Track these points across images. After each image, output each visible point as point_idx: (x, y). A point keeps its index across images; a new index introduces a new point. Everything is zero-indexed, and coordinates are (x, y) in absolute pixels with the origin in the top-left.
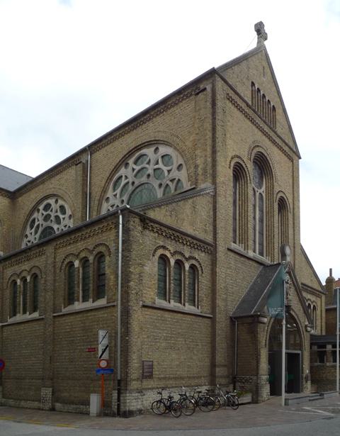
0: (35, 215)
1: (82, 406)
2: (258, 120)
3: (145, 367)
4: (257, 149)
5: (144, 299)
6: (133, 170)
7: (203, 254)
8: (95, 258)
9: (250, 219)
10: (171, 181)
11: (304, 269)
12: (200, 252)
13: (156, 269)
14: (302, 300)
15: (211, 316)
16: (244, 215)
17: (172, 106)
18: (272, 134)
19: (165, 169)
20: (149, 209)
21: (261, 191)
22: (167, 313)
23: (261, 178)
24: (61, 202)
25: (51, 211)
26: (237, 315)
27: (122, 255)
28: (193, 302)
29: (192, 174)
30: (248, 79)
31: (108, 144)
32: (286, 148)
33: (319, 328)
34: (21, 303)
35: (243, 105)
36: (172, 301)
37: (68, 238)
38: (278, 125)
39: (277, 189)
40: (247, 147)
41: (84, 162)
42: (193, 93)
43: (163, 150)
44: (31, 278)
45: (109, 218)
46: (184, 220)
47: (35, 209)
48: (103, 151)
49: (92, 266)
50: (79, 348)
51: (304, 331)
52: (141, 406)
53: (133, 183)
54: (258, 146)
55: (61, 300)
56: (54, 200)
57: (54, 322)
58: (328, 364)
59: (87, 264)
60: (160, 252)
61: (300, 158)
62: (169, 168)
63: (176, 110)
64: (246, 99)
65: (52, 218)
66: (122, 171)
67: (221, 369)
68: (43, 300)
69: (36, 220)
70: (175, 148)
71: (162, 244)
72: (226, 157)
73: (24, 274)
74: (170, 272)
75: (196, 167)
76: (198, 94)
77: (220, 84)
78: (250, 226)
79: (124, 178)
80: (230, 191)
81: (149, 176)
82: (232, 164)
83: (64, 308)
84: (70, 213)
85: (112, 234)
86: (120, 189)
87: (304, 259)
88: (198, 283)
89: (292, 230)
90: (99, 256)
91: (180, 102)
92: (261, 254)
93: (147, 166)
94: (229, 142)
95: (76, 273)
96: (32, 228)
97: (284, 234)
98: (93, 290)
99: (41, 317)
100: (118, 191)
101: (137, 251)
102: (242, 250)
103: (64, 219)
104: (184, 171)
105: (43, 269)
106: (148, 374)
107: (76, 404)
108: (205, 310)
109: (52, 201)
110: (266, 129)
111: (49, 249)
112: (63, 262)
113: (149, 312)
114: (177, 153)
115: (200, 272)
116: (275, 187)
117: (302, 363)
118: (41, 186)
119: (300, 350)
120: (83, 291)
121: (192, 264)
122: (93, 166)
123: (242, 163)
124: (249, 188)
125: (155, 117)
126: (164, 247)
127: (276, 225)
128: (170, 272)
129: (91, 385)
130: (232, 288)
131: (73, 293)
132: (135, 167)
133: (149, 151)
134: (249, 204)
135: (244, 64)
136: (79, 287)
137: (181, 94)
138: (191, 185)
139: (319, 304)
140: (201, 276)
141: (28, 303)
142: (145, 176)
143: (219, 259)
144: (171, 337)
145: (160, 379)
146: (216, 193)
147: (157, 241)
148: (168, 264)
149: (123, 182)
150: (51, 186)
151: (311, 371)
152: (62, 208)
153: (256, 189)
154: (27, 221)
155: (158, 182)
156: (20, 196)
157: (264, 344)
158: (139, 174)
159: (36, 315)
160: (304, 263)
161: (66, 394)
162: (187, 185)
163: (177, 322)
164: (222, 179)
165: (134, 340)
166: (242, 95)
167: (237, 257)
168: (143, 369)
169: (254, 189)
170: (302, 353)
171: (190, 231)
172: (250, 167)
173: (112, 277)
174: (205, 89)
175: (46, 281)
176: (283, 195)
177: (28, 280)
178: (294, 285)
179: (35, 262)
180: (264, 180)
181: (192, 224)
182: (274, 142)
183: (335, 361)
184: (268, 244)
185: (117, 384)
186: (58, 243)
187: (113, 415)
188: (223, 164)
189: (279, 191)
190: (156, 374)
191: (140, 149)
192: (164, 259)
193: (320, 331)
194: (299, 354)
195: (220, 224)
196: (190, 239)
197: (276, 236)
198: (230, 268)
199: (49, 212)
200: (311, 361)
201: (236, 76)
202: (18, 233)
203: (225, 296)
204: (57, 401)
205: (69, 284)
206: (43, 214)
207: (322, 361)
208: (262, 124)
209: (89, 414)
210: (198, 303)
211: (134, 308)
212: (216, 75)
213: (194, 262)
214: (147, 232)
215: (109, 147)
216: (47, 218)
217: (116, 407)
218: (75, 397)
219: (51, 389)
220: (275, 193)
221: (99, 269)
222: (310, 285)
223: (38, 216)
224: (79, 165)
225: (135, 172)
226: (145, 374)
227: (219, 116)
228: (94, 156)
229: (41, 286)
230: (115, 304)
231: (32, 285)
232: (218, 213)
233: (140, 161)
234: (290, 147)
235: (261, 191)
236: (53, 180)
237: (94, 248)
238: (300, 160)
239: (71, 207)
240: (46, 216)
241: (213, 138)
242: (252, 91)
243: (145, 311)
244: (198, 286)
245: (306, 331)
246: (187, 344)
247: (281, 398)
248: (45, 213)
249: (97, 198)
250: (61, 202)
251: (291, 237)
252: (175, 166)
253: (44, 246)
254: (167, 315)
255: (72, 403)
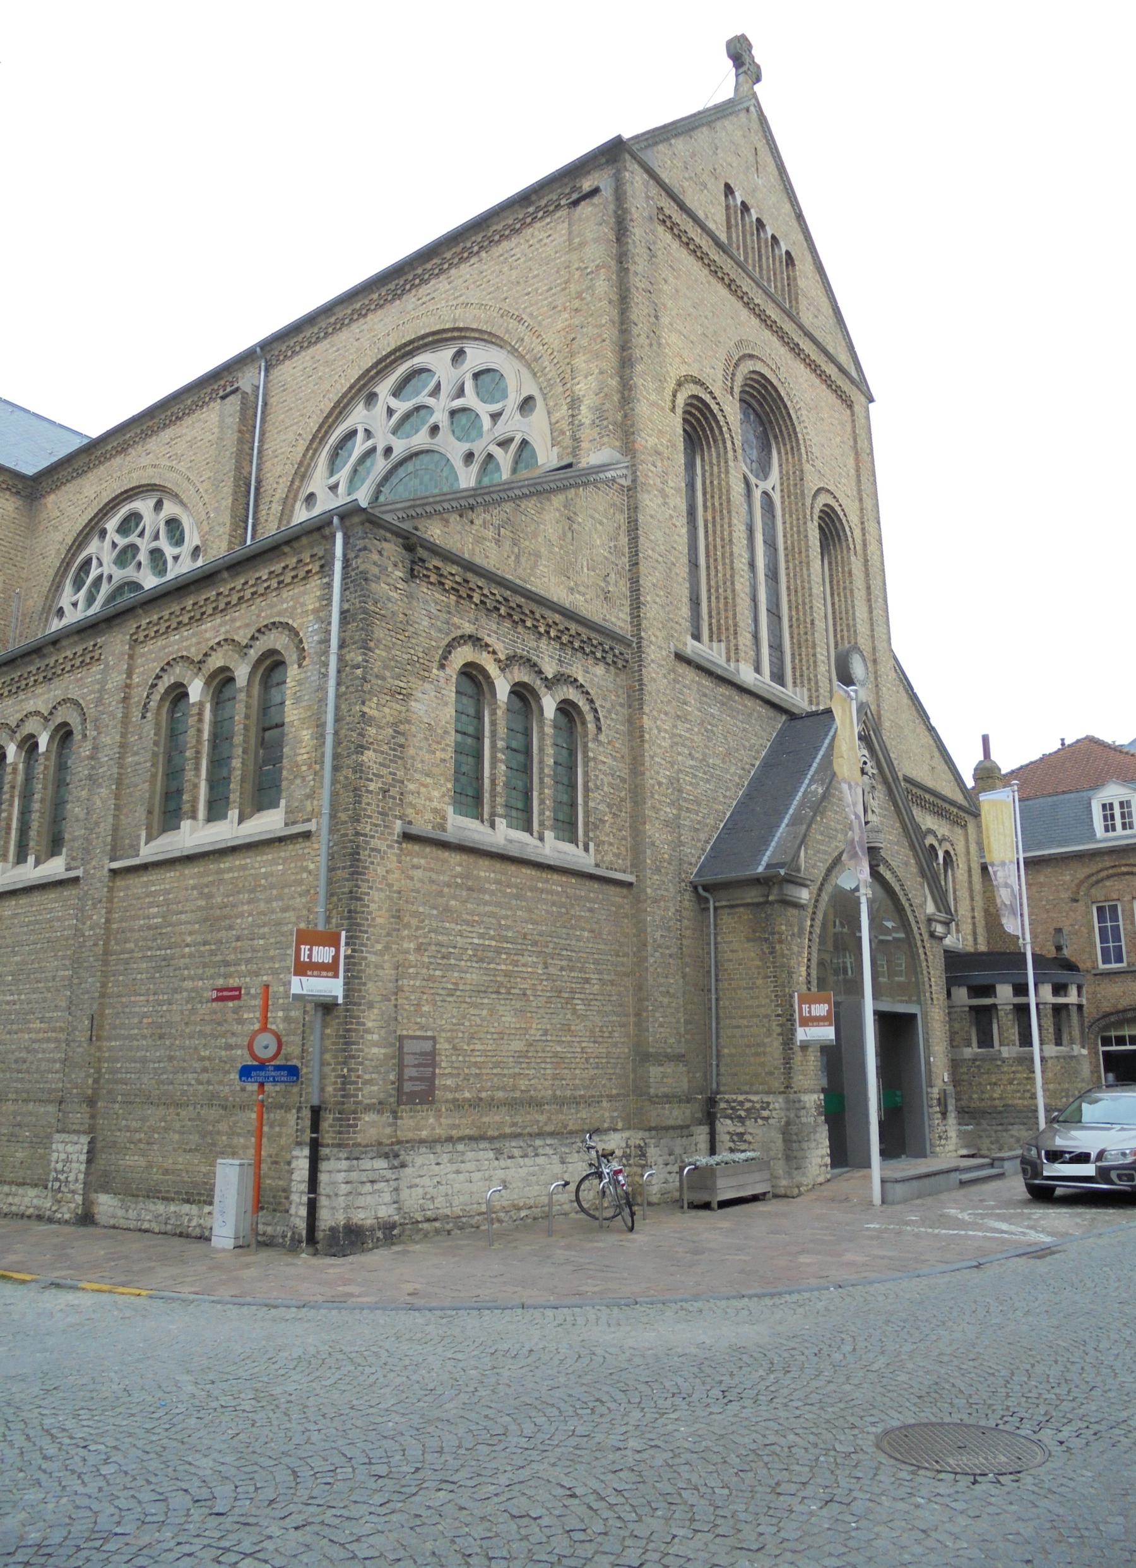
0: (92, 547)
1: (186, 1208)
2: (746, 285)
3: (408, 1060)
4: (749, 366)
5: (410, 811)
6: (390, 412)
7: (600, 670)
8: (252, 674)
9: (741, 564)
10: (499, 445)
11: (906, 732)
12: (591, 661)
13: (450, 712)
14: (913, 835)
15: (631, 878)
16: (720, 549)
17: (503, 237)
18: (788, 327)
19: (484, 410)
20: (429, 515)
21: (767, 485)
22: (484, 863)
23: (766, 448)
24: (170, 509)
25: (141, 535)
26: (708, 879)
27: (341, 659)
28: (567, 828)
29: (564, 425)
30: (714, 173)
31: (318, 340)
32: (830, 370)
33: (967, 928)
34: (14, 824)
35: (705, 243)
36: (501, 823)
37: (176, 608)
38: (803, 303)
39: (812, 483)
40: (722, 355)
41: (248, 389)
42: (563, 202)
43: (478, 356)
44: (52, 738)
45: (304, 541)
46: (538, 555)
47: (94, 528)
48: (304, 359)
49: (242, 696)
50: (188, 984)
51: (926, 936)
52: (391, 1210)
53: (388, 451)
54: (751, 356)
55: (141, 813)
56: (151, 503)
57: (111, 890)
58: (1006, 1052)
59: (227, 693)
60: (464, 655)
61: (871, 400)
62: (495, 407)
63: (516, 247)
64: (711, 225)
65: (143, 556)
66: (358, 416)
67: (669, 1069)
68: (82, 816)
69: (94, 562)
70: (514, 351)
71: (468, 628)
72: (661, 380)
73: (30, 727)
74: (493, 723)
75: (575, 403)
76: (575, 203)
77: (636, 180)
78: (742, 585)
79: (360, 435)
80: (677, 480)
81: (435, 430)
82: (681, 400)
83: (146, 844)
84: (197, 542)
85: (309, 594)
86: (348, 467)
87: (905, 700)
88: (586, 764)
89: (866, 609)
90: (268, 662)
91: (525, 225)
92: (778, 677)
93: (431, 401)
94: (671, 339)
95: (192, 721)
96: (78, 584)
97: (842, 620)
98: (243, 780)
99: (72, 874)
100: (343, 475)
101: (388, 649)
102: (722, 661)
103: (176, 558)
104: (539, 412)
105: (91, 711)
106: (419, 1087)
107: (167, 1199)
108: (609, 858)
109: (143, 506)
110: (773, 312)
111: (116, 643)
112: (154, 686)
113: (422, 857)
114: (517, 365)
115: (591, 726)
116: (808, 477)
117: (927, 1047)
118: (117, 461)
119: (919, 1002)
120: (212, 784)
121: (565, 701)
122: (272, 401)
123: (707, 398)
124: (732, 471)
125: (457, 265)
126: (475, 640)
127: (817, 590)
128: (493, 723)
129: (223, 1127)
130: (695, 786)
131: (179, 792)
132: (394, 403)
133: (438, 360)
134: (735, 521)
135: (703, 136)
136: (197, 769)
137: (530, 204)
138: (560, 457)
139: (960, 847)
140: (596, 739)
141: (35, 825)
142: (424, 431)
143: (650, 687)
144: (498, 951)
145: (458, 1105)
146: (634, 481)
147: (456, 620)
148: (488, 696)
149: (359, 446)
150: (145, 461)
151: (956, 1081)
152: (173, 524)
153: (753, 480)
154: (66, 564)
155: (465, 447)
156: (52, 491)
157: (802, 979)
158: (407, 427)
159: (55, 867)
160: (908, 714)
161: (134, 1160)
162: (547, 457)
163: (517, 897)
164: (652, 441)
165: (372, 958)
166: (701, 214)
167: (706, 682)
168: (401, 1066)
169: (745, 478)
170: (925, 1014)
171: (558, 593)
172: (731, 411)
173: (306, 735)
174: (595, 191)
175: (95, 748)
176: (832, 502)
177: (42, 748)
178: (885, 782)
179: (68, 686)
180: (774, 446)
181: (565, 571)
182: (796, 350)
183: (1026, 1040)
184: (797, 645)
185: (308, 1123)
186: (144, 622)
187: (293, 1247)
188: (653, 397)
189: (820, 490)
190: (446, 1088)
191: (411, 354)
192: (473, 676)
193: (970, 938)
194: (913, 1017)
195: (650, 578)
196: (557, 618)
197: (820, 624)
198: (682, 718)
199: (133, 538)
200: (954, 1041)
201: (680, 164)
202: (35, 601)
203: (671, 812)
204: (105, 1188)
205: (169, 759)
206: (114, 545)
207: (985, 1040)
208: (759, 299)
209: (209, 1239)
210: (586, 834)
211: (375, 843)
212: (627, 157)
213: (572, 694)
214: (422, 589)
215: (325, 344)
216: (126, 555)
217: (303, 1212)
218: (166, 1172)
219: (84, 1139)
220: (809, 494)
221: (265, 708)
222: (930, 784)
223: (101, 551)
224: (231, 398)
225: (396, 417)
226: (408, 1087)
227: (639, 265)
228: (276, 373)
229: (79, 768)
230: (312, 826)
231: (52, 763)
232: (642, 540)
233: (409, 388)
234: (841, 369)
235: (767, 485)
236: (153, 444)
237: (253, 638)
238: (871, 406)
239: (199, 524)
240: (124, 550)
241: (622, 323)
242: (728, 207)
243: (409, 854)
244: (586, 774)
245: (932, 935)
246: (550, 977)
247: (868, 1178)
248: (122, 542)
249: (280, 494)
250: (170, 509)
251: (862, 629)
252: (513, 400)
253: (101, 633)
254: (485, 870)
255: (153, 1194)
